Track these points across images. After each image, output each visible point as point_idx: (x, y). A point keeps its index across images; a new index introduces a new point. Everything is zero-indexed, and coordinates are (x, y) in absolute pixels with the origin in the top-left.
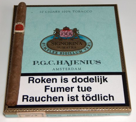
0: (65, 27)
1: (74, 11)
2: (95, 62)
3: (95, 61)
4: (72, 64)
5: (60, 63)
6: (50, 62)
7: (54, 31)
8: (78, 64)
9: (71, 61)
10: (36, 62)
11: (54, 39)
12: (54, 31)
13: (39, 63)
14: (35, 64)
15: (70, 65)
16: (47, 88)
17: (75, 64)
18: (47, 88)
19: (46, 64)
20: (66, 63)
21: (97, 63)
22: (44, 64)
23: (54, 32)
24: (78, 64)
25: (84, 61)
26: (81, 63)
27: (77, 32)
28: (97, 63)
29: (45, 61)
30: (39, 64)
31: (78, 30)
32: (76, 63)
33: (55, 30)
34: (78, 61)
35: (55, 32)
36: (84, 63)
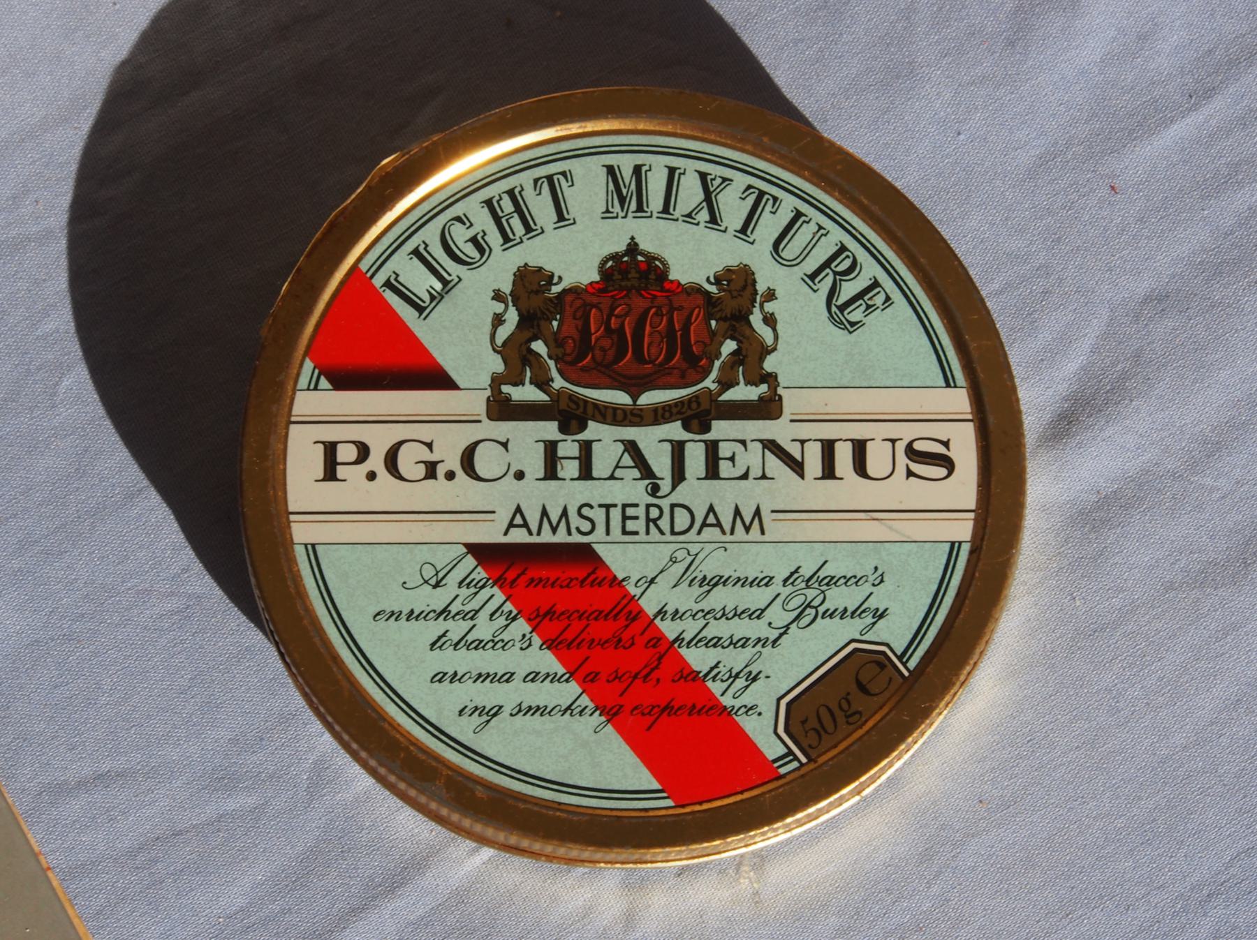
0: (621, 247)
1: (764, 477)
2: (902, 460)
3: (900, 446)
4: (679, 475)
5: (570, 469)
6: (480, 450)
7: (498, 296)
8: (745, 476)
10: (346, 453)
12: (498, 296)
13: (376, 461)
14: (341, 471)
15: (665, 486)
17: (712, 472)
19: (441, 470)
20: (627, 460)
22: (421, 471)
23: (498, 320)
24: (745, 476)
25: (794, 450)
26: (773, 463)
27: (756, 319)
28: (916, 467)
29: (429, 446)
30: (372, 476)
31: (771, 295)
32: (725, 468)
33: (507, 288)
35: (512, 317)
36: (797, 467)
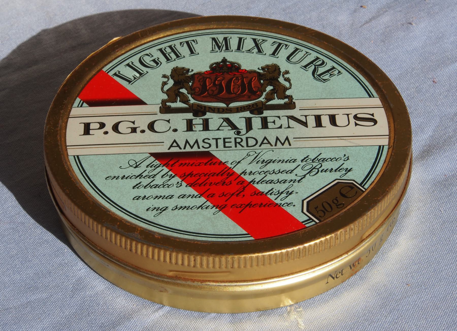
3: (351, 117)
8: (281, 127)
9: (217, 139)
11: (217, 68)
14: (91, 132)
16: (226, 140)
18: (226, 140)
19: (138, 130)
20: (225, 124)
21: (358, 122)
22: (130, 130)
24: (281, 127)
28: (358, 122)
29: (133, 123)
31: (287, 72)
32: (270, 125)
34: (277, 119)
